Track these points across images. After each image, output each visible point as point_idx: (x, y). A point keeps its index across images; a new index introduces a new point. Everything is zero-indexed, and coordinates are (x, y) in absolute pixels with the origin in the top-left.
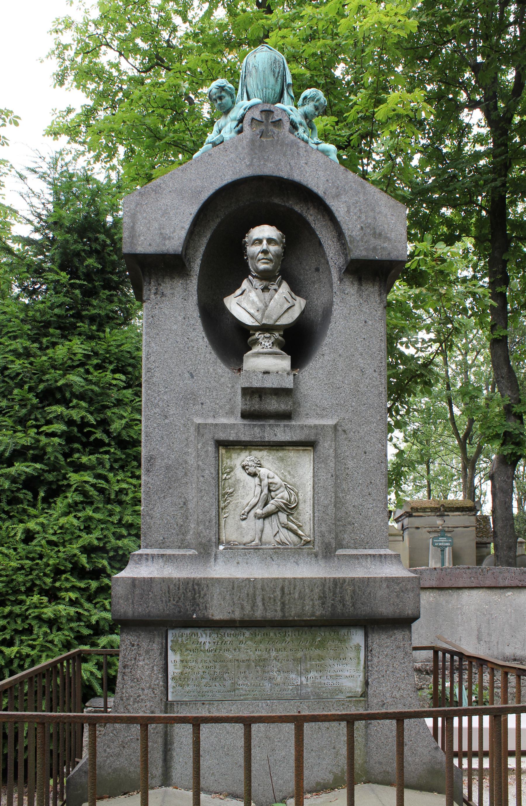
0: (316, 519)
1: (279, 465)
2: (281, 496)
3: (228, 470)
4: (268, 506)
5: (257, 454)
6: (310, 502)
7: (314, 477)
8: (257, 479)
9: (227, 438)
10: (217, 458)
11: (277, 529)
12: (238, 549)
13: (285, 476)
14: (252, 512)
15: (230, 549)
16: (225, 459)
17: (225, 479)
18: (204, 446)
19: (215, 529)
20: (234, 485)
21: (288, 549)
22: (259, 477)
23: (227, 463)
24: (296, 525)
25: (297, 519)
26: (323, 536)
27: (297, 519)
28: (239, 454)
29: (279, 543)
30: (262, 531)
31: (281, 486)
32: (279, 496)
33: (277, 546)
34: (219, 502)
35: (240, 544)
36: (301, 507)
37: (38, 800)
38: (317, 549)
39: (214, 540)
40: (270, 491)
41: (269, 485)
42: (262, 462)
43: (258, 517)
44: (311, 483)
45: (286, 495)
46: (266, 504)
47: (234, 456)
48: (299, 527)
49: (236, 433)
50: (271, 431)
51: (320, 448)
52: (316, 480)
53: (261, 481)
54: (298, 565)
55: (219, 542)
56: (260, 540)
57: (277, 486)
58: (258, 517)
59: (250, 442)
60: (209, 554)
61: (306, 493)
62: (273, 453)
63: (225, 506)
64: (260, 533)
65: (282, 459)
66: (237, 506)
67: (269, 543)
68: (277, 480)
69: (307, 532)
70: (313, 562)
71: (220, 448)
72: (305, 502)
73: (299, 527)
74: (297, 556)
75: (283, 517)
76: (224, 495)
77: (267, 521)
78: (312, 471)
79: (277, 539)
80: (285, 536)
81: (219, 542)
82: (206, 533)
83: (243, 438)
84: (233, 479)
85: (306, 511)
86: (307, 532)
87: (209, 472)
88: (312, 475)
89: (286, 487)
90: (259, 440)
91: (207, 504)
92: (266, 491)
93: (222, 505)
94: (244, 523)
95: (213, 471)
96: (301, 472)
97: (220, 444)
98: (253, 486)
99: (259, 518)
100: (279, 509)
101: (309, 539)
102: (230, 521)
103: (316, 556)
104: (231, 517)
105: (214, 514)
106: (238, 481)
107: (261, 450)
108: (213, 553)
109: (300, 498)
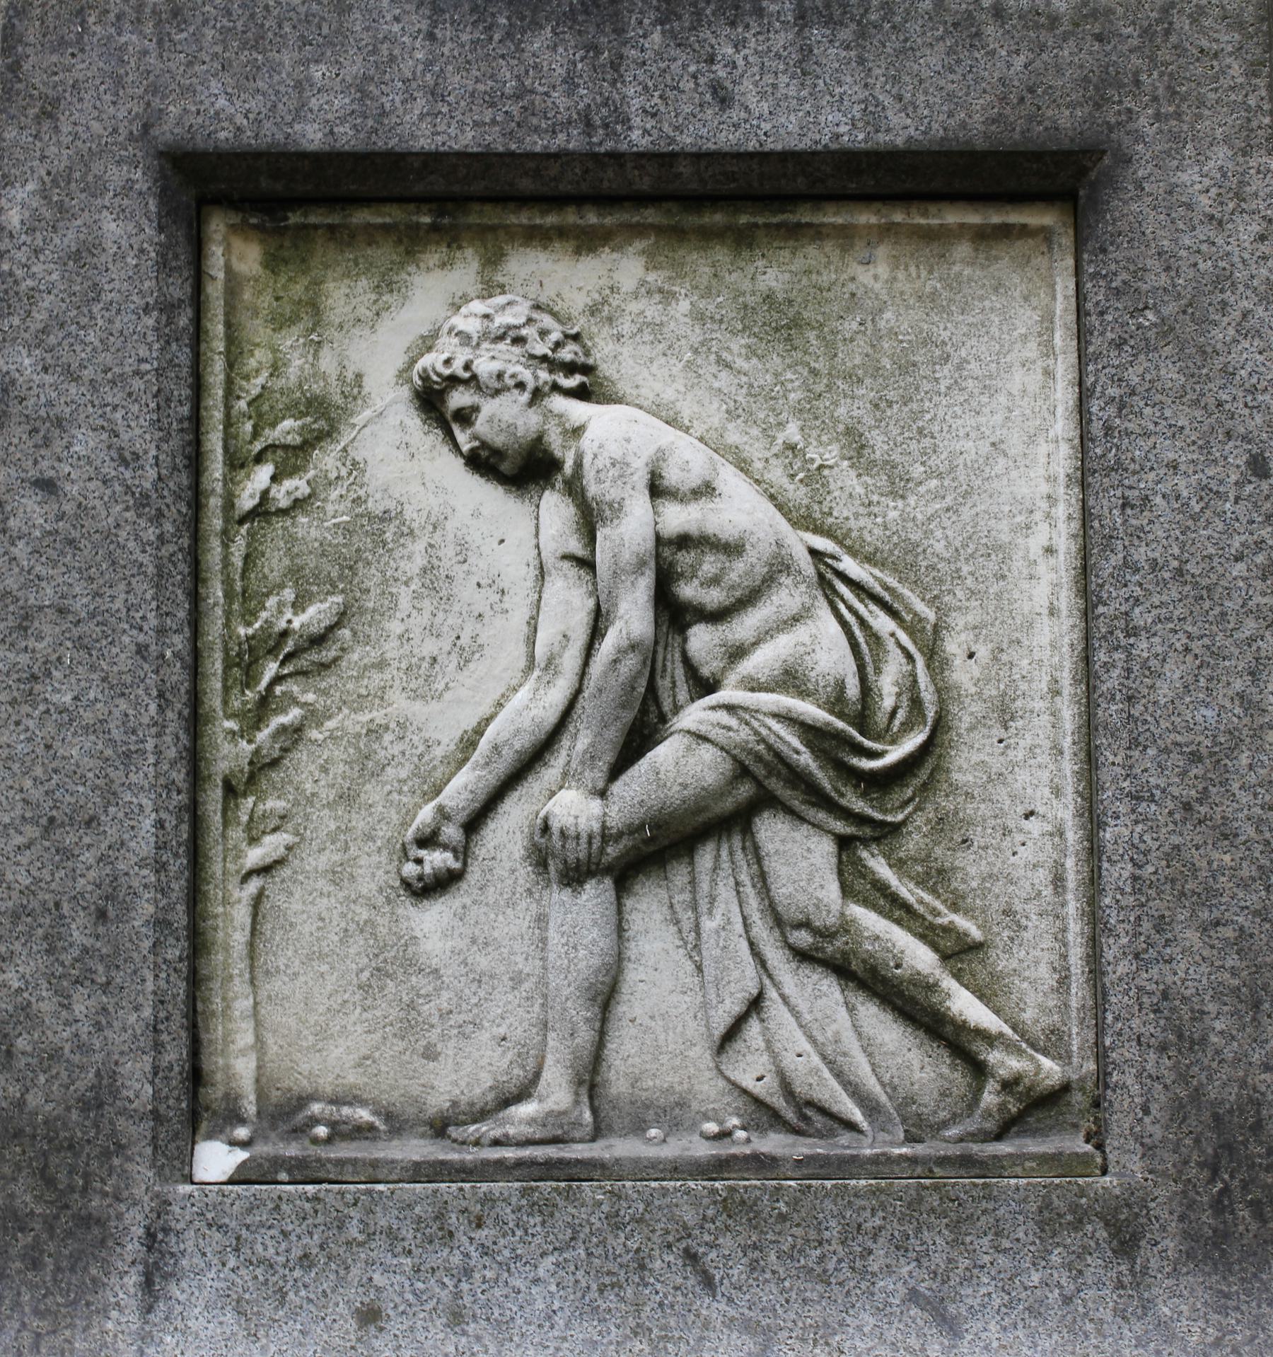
0: (1117, 873)
1: (761, 372)
2: (788, 655)
3: (287, 429)
4: (664, 754)
5: (560, 280)
6: (1049, 721)
7: (1083, 477)
8: (555, 510)
9: (270, 134)
10: (185, 308)
11: (745, 979)
12: (373, 1172)
13: (816, 477)
14: (513, 820)
15: (304, 1172)
16: (257, 329)
17: (263, 511)
18: (58, 200)
19: (148, 987)
20: (344, 570)
21: (846, 1166)
22: (574, 489)
23: (281, 359)
24: (929, 934)
25: (935, 877)
26: (1184, 1040)
27: (935, 877)
28: (386, 285)
29: (762, 1114)
30: (605, 996)
31: (779, 567)
32: (762, 661)
33: (744, 1143)
34: (196, 721)
35: (396, 1124)
36: (969, 760)
37: (852, 738)
38: (1126, 1169)
39: (138, 1085)
40: (673, 613)
41: (668, 559)
42: (603, 352)
43: (562, 863)
44: (1063, 536)
45: (824, 647)
46: (639, 737)
47: (344, 295)
48: (959, 953)
49: (361, 89)
50: (682, 64)
51: (1135, 210)
52: (1106, 505)
53: (589, 519)
54: (950, 1326)
55: (197, 1103)
56: (590, 1078)
57: (738, 571)
58: (562, 863)
59: (483, 161)
60: (89, 1234)
61: (1019, 629)
62: (701, 263)
63: (261, 767)
64: (581, 1014)
65: (782, 325)
66: (366, 765)
67: (675, 1113)
68: (740, 510)
69: (1029, 996)
70: (1100, 1300)
71: (217, 225)
72: (1005, 713)
73: (959, 953)
74: (938, 1241)
75: (800, 858)
76: (244, 663)
77: (649, 907)
78: (1063, 426)
79: (750, 1069)
80: (825, 1038)
81: (197, 1103)
82: (65, 1021)
83: (423, 129)
84: (336, 508)
85: (1019, 800)
86: (1029, 996)
87: (104, 442)
88: (1063, 460)
89: (827, 579)
90: (572, 140)
91: (75, 749)
92: (634, 616)
93: (229, 752)
94: (431, 922)
95: (138, 434)
96: (963, 433)
97: (210, 187)
98: (518, 574)
99: (574, 876)
100: (759, 789)
101: (1050, 1070)
102: (306, 906)
103: (1126, 1240)
104: (317, 861)
105: (144, 841)
106: (379, 528)
107: (587, 242)
108: (135, 1222)
109: (963, 675)
